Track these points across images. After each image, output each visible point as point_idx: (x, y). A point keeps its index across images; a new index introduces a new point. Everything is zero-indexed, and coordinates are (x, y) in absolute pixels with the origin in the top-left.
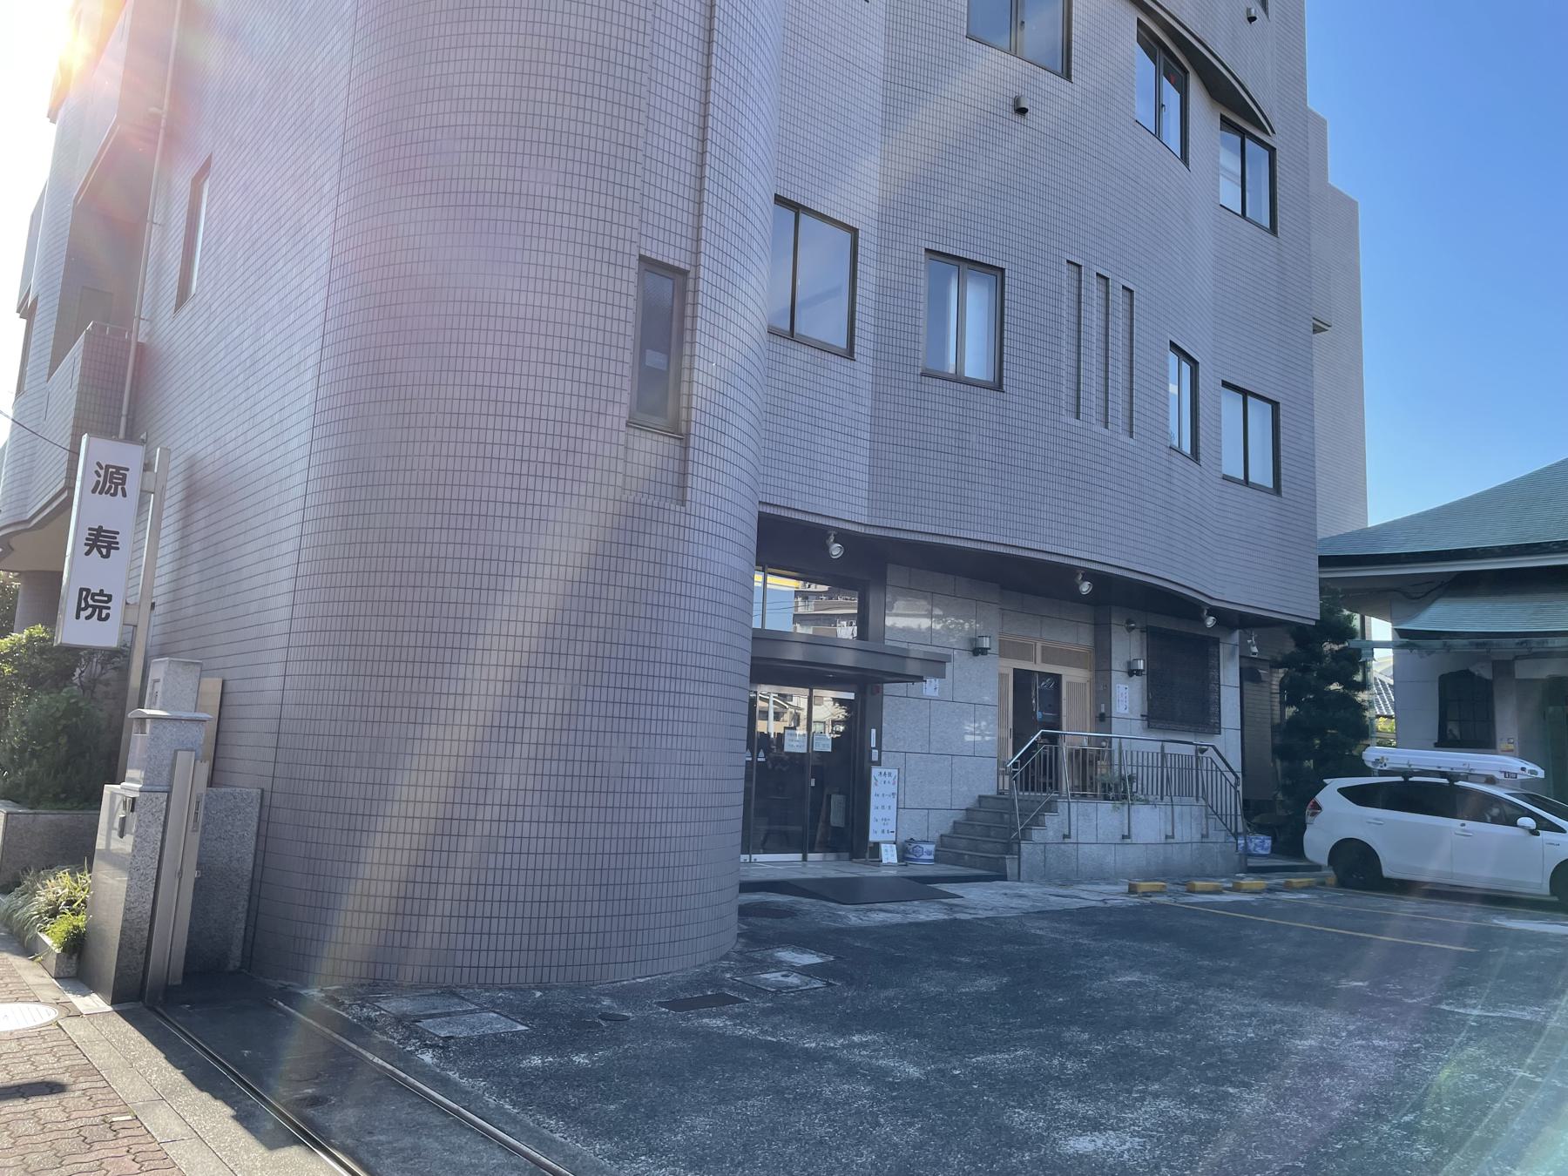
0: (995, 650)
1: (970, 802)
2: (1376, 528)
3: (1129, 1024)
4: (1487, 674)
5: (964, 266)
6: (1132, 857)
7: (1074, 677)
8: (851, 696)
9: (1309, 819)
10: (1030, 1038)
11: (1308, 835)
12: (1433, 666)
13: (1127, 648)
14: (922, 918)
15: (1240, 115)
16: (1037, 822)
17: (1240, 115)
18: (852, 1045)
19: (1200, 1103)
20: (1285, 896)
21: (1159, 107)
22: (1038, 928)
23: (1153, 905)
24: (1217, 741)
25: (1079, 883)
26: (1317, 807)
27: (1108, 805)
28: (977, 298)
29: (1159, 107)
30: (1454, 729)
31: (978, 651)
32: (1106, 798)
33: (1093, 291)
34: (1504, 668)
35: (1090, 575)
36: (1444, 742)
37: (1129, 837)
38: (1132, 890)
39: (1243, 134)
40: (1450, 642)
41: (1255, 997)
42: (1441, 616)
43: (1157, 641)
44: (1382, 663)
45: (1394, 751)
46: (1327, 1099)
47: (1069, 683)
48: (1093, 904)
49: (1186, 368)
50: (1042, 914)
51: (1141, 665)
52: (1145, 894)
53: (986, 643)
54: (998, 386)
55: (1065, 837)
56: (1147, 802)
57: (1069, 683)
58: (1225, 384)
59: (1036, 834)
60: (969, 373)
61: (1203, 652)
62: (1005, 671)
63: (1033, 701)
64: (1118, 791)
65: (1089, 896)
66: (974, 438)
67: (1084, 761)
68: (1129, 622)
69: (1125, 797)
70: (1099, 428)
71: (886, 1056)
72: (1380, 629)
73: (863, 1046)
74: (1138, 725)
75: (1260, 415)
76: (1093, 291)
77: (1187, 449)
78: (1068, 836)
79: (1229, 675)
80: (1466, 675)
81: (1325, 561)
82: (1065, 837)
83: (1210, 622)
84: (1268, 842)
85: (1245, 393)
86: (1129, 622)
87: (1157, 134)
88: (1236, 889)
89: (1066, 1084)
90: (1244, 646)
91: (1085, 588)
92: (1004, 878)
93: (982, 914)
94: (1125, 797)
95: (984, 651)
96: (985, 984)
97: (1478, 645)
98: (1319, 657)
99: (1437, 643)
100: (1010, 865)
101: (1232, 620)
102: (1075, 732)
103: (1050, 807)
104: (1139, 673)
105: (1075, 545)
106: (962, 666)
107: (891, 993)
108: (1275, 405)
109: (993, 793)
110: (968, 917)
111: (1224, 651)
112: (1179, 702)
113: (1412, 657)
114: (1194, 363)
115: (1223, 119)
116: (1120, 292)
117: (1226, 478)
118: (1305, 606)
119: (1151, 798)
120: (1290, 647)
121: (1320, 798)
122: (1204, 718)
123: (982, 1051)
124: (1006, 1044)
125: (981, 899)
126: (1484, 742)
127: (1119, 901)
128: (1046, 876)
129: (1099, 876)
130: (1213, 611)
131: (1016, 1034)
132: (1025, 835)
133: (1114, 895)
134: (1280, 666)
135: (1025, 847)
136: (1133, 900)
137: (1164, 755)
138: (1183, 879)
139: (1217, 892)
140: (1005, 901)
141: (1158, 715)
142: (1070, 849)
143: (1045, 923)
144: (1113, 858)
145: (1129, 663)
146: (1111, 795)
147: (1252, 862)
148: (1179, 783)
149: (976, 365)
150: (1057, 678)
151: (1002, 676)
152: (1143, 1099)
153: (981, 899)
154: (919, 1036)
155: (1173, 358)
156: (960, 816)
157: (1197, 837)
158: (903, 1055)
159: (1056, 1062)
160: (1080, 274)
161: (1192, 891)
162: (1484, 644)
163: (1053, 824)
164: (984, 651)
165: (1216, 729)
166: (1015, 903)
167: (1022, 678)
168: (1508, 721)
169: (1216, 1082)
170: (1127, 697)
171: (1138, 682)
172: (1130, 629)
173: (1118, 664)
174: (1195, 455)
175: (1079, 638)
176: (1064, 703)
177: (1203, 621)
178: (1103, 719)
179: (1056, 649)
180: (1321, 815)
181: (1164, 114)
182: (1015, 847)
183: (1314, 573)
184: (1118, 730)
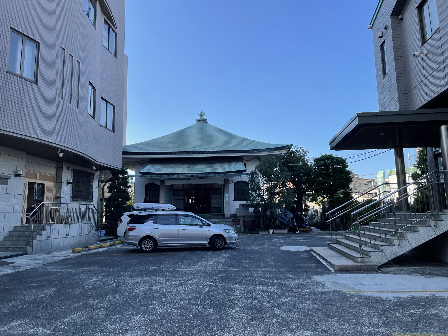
0: (24, 175)
1: (11, 229)
2: (129, 145)
3: (106, 294)
4: (158, 184)
5: (25, 38)
6: (70, 241)
7: (49, 185)
8: (411, 200)
9: (119, 224)
10: (79, 307)
11: (119, 229)
12: (144, 181)
13: (67, 175)
14: (5, 272)
15: (109, 21)
16: (39, 233)
17: (109, 21)
18: (13, 328)
19: (147, 313)
20: (115, 247)
21: (89, 8)
22: (51, 269)
23: (82, 255)
24: (91, 203)
25: (53, 252)
26: (121, 221)
27: (62, 226)
28: (29, 50)
29: (89, 8)
30: (148, 198)
31: (17, 175)
32: (62, 223)
33: (68, 58)
34: (162, 182)
35: (62, 151)
36: (146, 202)
37: (69, 235)
38: (73, 252)
39: (109, 26)
40: (152, 175)
41: (134, 277)
42: (149, 169)
43: (76, 174)
44: (132, 182)
45: (139, 205)
46: (177, 302)
47: (47, 187)
48: (63, 258)
49: (93, 90)
50: (49, 264)
51: (71, 181)
52: (78, 252)
53: (21, 173)
54: (36, 82)
55: (48, 237)
56: (75, 224)
57: (47, 187)
58: (102, 98)
59: (38, 238)
60: (25, 76)
61: (89, 177)
62: (25, 182)
63: (35, 193)
64: (66, 221)
65: (61, 255)
66: (26, 99)
67: (53, 212)
68: (68, 167)
69: (68, 223)
70: (69, 104)
71: (30, 328)
72: (131, 172)
73: (18, 326)
74: (69, 200)
75: (110, 108)
76: (68, 58)
77: (92, 115)
78: (50, 237)
79: (96, 183)
80: (153, 184)
81: (124, 153)
82: (48, 237)
83: (94, 168)
84: (104, 232)
85: (107, 102)
86: (68, 167)
87: (88, 15)
88: (102, 247)
89: (104, 320)
90: (100, 176)
91: (61, 155)
92: (26, 254)
93: (29, 267)
94: (68, 223)
95: (20, 175)
96: (48, 292)
97: (159, 176)
98: (118, 179)
99: (149, 176)
100: (29, 249)
101: (101, 168)
102: (49, 201)
103: (44, 228)
104: (70, 183)
105: (60, 141)
106: (13, 181)
107: (14, 303)
108: (114, 107)
109: (20, 225)
110: (24, 269)
111: (95, 177)
112: (81, 192)
113: (142, 179)
114: (95, 90)
115: (105, 20)
116: (77, 62)
117: (101, 126)
118: (118, 164)
119: (75, 222)
120: (110, 176)
121: (122, 218)
122: (88, 197)
123: (65, 316)
124: (72, 312)
125: (23, 262)
126: (157, 201)
127: (71, 256)
128: (42, 251)
129: (59, 249)
130: (95, 165)
131: (73, 307)
132: (34, 238)
133: (66, 254)
134: (108, 181)
135: (35, 242)
136: (75, 255)
137: (80, 208)
138: (86, 245)
139: (97, 248)
140: (32, 262)
141: (75, 196)
142: (49, 241)
143: (53, 267)
144: (63, 242)
145: (67, 180)
146: (64, 222)
147: (102, 238)
148: (83, 217)
149: (28, 73)
150: (43, 185)
151: (25, 185)
152: (130, 317)
153: (23, 262)
154: (37, 317)
155: (90, 87)
156: (6, 234)
157: (87, 233)
158: (36, 325)
159: (94, 313)
160: (65, 52)
161: (90, 249)
162: (160, 176)
163: (44, 233)
164: (20, 175)
165: (92, 200)
166: (36, 262)
167: (31, 185)
168: (162, 196)
169: (146, 305)
170: (67, 191)
171: (70, 186)
172: (68, 170)
173: (64, 181)
174: (94, 117)
175: (51, 172)
176: (45, 193)
177: (92, 168)
178: (58, 198)
179: (44, 174)
180: (123, 223)
181: (90, 11)
182: (31, 243)
183: (121, 156)
184: (63, 201)
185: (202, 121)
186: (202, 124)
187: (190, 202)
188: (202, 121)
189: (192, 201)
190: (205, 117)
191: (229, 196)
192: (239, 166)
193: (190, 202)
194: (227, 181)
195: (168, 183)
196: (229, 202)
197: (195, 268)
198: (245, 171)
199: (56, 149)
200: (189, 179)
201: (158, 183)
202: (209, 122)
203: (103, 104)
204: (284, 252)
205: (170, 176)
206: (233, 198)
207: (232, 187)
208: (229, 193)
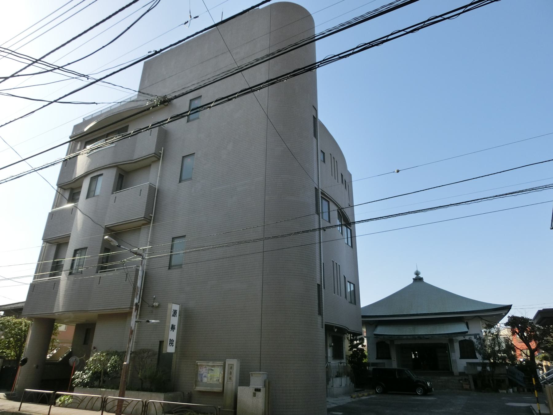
35: (336, 327)
42: (380, 330)
75: (352, 286)
87: (342, 233)
185: (418, 279)
186: (418, 283)
187: (413, 357)
188: (418, 279)
189: (415, 355)
190: (421, 276)
191: (456, 354)
192: (461, 328)
193: (413, 357)
194: (451, 341)
195: (399, 342)
196: (455, 361)
197: (443, 411)
198: (467, 332)
199: (333, 326)
200: (416, 339)
201: (389, 343)
202: (425, 280)
203: (348, 284)
204: (509, 406)
205: (399, 337)
206: (459, 356)
207: (457, 346)
208: (454, 352)
